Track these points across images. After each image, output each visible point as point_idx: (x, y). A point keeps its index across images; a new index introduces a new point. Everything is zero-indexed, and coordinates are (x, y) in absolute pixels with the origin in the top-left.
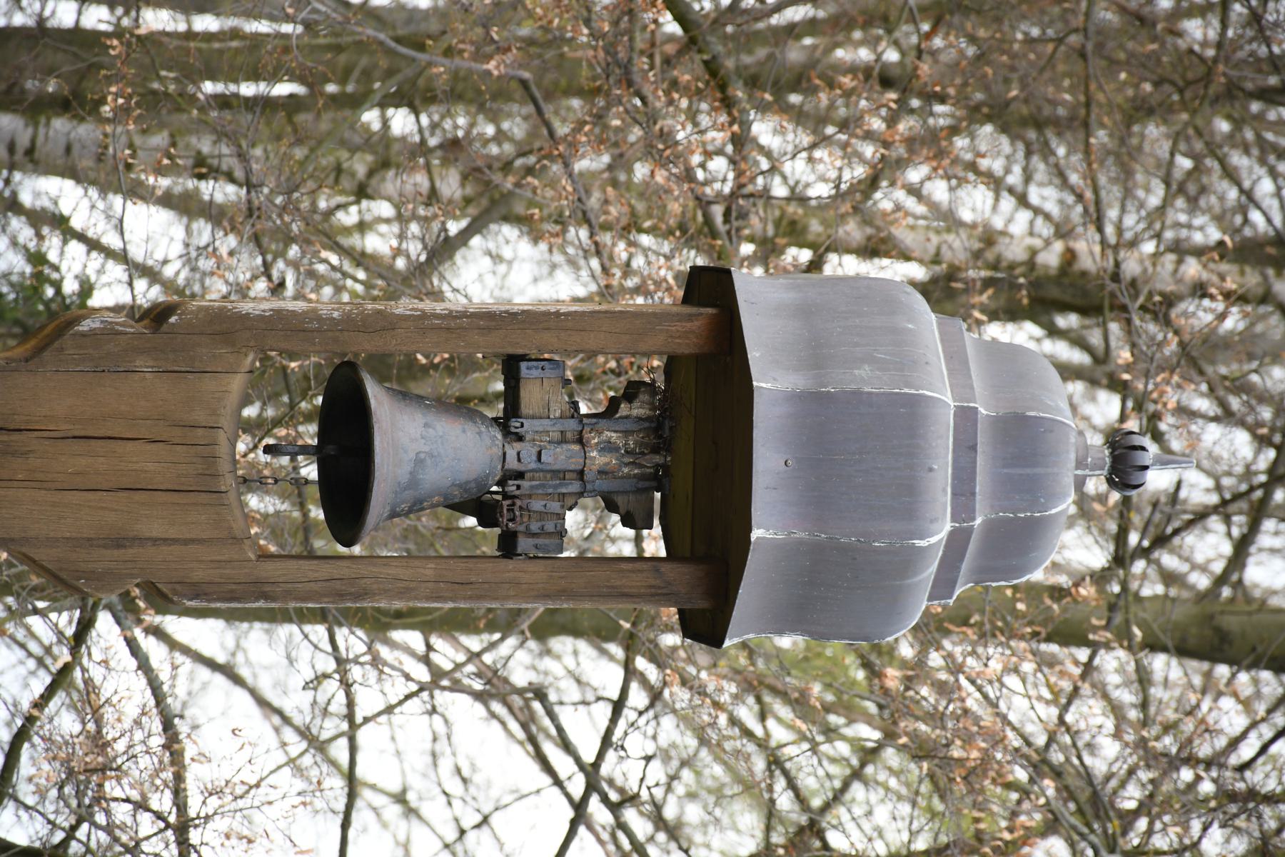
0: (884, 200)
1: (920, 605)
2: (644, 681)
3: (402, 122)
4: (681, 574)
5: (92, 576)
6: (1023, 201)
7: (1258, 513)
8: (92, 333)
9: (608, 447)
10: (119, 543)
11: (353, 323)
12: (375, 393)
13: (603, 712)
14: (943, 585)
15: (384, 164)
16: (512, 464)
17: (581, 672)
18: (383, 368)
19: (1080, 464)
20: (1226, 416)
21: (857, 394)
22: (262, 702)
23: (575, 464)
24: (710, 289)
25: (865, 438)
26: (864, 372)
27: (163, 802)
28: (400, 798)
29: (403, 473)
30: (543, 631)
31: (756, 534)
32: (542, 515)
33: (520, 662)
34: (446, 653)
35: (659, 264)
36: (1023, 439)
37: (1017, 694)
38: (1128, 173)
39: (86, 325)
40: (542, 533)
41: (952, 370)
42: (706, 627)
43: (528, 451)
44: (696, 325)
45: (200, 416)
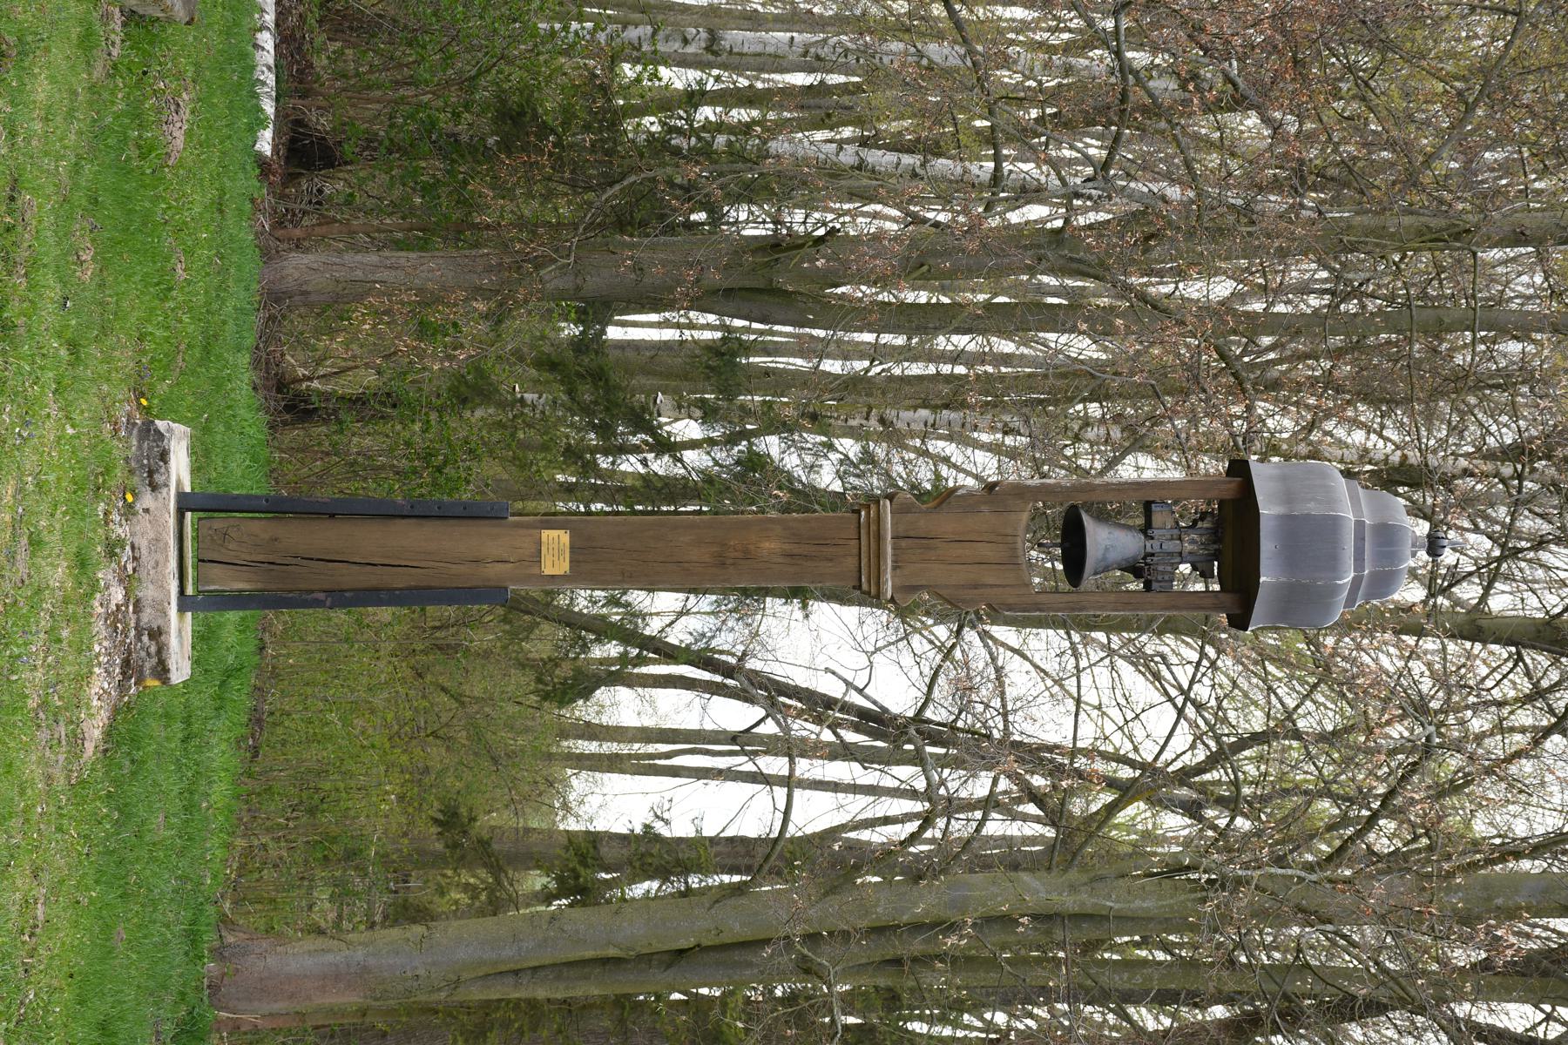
0: (1315, 436)
1: (1339, 612)
2: (1208, 658)
3: (1094, 409)
4: (1227, 598)
5: (964, 601)
6: (1381, 436)
7: (1494, 577)
8: (962, 496)
9: (1193, 542)
10: (975, 587)
11: (1075, 489)
12: (1086, 518)
13: (1190, 669)
14: (1350, 601)
15: (1087, 424)
16: (1149, 550)
17: (1181, 652)
18: (1089, 508)
19: (1414, 545)
20: (1476, 530)
21: (1308, 515)
22: (1036, 667)
23: (1178, 549)
24: (1239, 469)
25: (1312, 537)
26: (1311, 505)
27: (996, 703)
28: (1099, 707)
29: (1100, 554)
30: (1160, 633)
31: (1262, 579)
32: (1163, 573)
33: (1150, 643)
34: (1116, 642)
35: (1212, 466)
36: (1387, 535)
37: (1384, 657)
38: (1431, 423)
39: (960, 492)
40: (1163, 581)
41: (1352, 506)
42: (1240, 621)
43: (1156, 544)
44: (1233, 485)
45: (1010, 531)
